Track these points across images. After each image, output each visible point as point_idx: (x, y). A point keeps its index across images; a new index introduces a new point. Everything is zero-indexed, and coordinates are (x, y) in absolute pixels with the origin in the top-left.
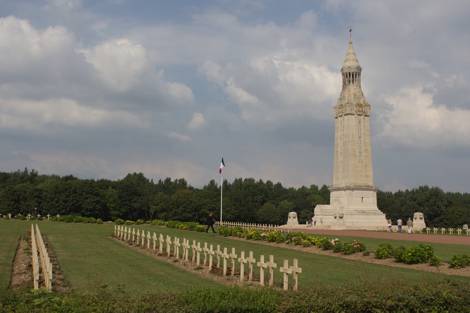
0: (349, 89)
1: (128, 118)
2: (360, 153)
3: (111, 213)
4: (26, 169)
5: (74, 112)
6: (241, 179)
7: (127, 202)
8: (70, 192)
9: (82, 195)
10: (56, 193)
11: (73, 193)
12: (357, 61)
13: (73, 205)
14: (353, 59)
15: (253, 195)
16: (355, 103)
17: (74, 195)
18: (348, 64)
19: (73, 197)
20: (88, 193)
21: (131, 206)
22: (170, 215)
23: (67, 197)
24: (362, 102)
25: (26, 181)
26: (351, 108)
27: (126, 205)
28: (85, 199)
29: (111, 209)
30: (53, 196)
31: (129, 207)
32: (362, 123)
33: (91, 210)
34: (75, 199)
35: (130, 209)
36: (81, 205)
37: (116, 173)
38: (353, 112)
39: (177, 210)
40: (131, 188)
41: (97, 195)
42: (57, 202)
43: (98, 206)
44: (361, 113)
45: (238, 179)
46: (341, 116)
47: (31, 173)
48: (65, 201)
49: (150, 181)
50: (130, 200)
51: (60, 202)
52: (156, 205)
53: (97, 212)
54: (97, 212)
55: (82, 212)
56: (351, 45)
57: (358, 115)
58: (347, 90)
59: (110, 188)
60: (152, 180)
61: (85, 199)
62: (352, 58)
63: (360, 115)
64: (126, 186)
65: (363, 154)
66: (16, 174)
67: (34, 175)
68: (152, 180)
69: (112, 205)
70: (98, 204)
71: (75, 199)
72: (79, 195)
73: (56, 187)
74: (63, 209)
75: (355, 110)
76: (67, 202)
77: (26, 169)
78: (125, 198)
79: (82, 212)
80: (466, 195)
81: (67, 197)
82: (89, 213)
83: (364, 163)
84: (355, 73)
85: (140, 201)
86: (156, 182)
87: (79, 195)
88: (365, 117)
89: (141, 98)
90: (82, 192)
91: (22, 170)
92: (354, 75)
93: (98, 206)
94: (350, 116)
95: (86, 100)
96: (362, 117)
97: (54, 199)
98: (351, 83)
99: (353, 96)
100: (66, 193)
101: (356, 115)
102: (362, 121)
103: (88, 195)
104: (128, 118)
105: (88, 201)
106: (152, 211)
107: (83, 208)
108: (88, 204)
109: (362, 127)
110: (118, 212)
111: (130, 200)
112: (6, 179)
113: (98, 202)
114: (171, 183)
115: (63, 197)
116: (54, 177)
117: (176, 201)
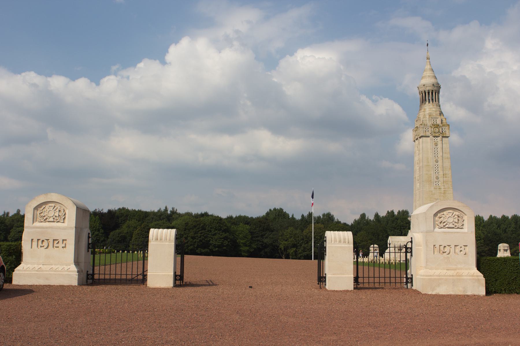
0: (425, 109)
1: (333, 147)
2: (437, 178)
3: (241, 248)
4: (166, 208)
5: (270, 144)
6: (392, 212)
7: (259, 238)
8: (199, 228)
9: (211, 231)
10: (185, 230)
11: (202, 230)
12: (436, 78)
13: (201, 241)
14: (429, 76)
15: (401, 229)
16: (429, 124)
17: (203, 231)
18: (424, 81)
19: (201, 233)
20: (217, 230)
21: (263, 242)
22: (300, 251)
23: (195, 233)
24: (439, 122)
25: (163, 219)
26: (425, 130)
27: (258, 241)
28: (214, 235)
29: (242, 245)
30: (182, 233)
31: (261, 243)
32: (440, 145)
33: (219, 247)
34: (203, 236)
35: (262, 245)
36: (209, 241)
37: (256, 209)
38: (428, 134)
39: (306, 245)
40: (265, 223)
41: (225, 231)
42: (186, 238)
43: (226, 242)
44: (437, 135)
45: (390, 211)
46: (417, 139)
47: (171, 211)
48: (193, 238)
49: (291, 216)
50: (262, 236)
51: (189, 238)
52: (286, 241)
53: (225, 248)
54: (225, 248)
55: (210, 248)
56: (428, 60)
57: (434, 137)
58: (422, 111)
59: (241, 224)
60: (293, 215)
61: (214, 235)
62: (428, 74)
63: (437, 137)
64: (259, 222)
65: (441, 179)
66: (153, 213)
67: (174, 212)
68: (293, 215)
69: (241, 241)
70: (227, 240)
71: (203, 236)
72: (208, 231)
73: (187, 224)
74: (191, 245)
75: (430, 132)
76: (195, 238)
77: (166, 208)
78: (257, 234)
79: (210, 248)
80: (515, 218)
81: (195, 233)
82: (217, 249)
83: (443, 189)
84: (423, 92)
85: (271, 236)
86: (298, 217)
87: (208, 231)
88: (443, 139)
89: (335, 122)
90: (211, 228)
91: (163, 209)
92: (430, 93)
93: (226, 242)
94: (424, 138)
95: (278, 128)
96: (439, 139)
97: (183, 235)
98: (427, 102)
99: (428, 117)
100: (194, 230)
101: (431, 137)
102: (440, 143)
103: (216, 232)
104: (333, 147)
105: (216, 237)
106: (282, 247)
107: (211, 244)
108: (216, 241)
109: (439, 150)
110: (247, 248)
111: (262, 236)
112: (146, 217)
113: (226, 238)
114: (368, 222)
115: (192, 234)
116: (189, 214)
117: (306, 236)
